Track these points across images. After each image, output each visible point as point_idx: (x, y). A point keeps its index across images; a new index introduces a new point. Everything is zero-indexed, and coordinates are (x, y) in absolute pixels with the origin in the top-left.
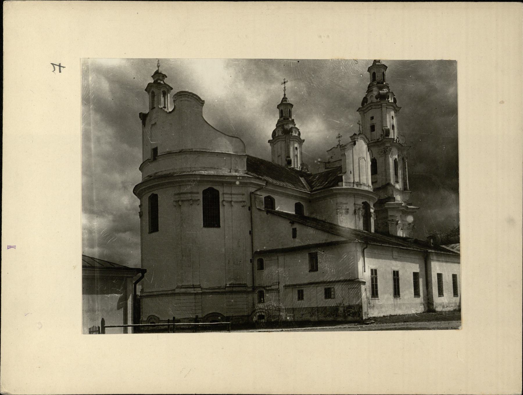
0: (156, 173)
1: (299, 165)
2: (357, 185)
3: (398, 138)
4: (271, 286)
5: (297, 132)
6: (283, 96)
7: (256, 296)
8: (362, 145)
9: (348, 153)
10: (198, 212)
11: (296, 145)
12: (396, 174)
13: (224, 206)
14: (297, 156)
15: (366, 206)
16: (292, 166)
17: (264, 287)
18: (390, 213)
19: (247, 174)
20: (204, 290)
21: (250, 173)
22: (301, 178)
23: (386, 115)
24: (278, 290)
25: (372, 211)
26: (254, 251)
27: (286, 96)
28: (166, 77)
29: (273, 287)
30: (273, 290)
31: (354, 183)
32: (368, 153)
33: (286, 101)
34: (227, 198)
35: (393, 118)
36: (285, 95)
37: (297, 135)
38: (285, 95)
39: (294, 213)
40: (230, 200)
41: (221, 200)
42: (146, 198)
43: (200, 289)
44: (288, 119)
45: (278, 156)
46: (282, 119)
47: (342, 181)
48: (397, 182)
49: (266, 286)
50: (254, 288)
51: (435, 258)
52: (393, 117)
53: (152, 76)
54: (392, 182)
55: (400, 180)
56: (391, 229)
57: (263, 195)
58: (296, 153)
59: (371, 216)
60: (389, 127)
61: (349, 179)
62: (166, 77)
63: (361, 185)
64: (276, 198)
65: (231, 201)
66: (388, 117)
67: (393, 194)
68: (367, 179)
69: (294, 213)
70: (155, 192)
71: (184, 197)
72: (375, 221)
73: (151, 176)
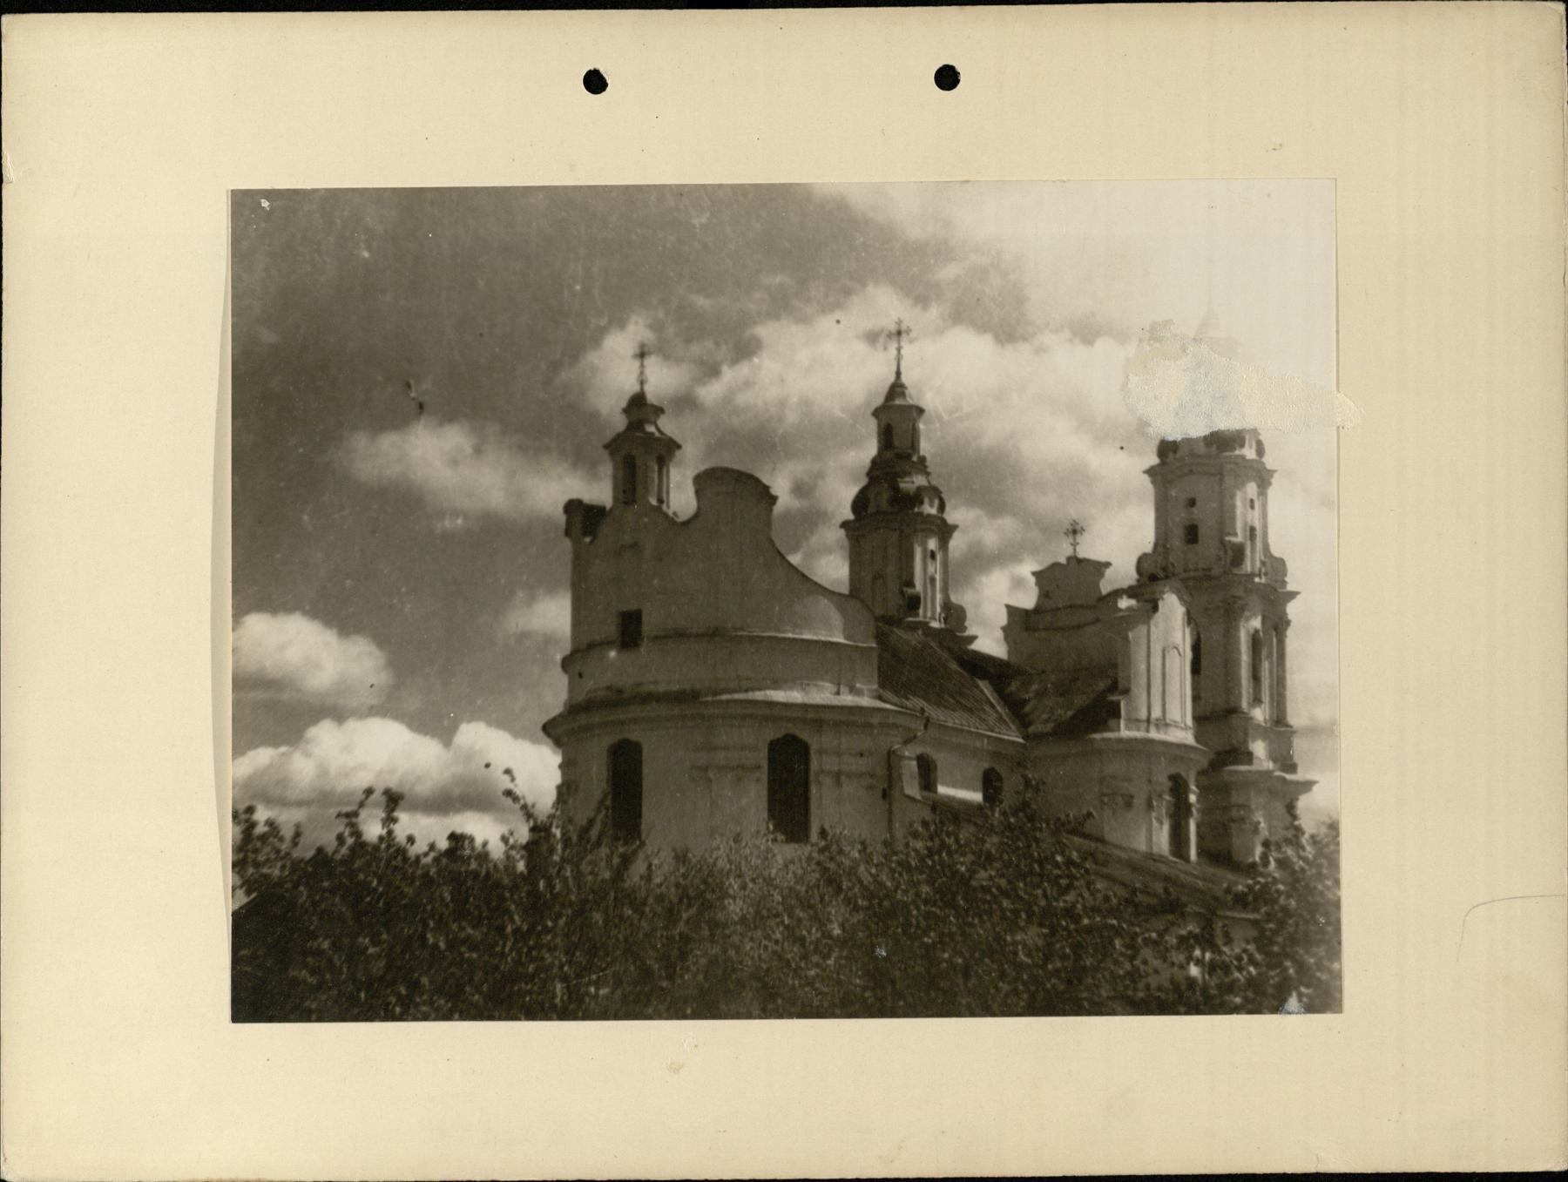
0: (639, 685)
1: (938, 609)
2: (1157, 726)
3: (1263, 563)
5: (937, 502)
6: (892, 379)
8: (1172, 607)
9: (1136, 634)
10: (752, 800)
11: (932, 544)
12: (1256, 677)
13: (820, 784)
14: (933, 580)
15: (1178, 787)
16: (920, 619)
18: (1236, 798)
19: (880, 698)
21: (888, 695)
23: (1233, 497)
25: (1193, 798)
27: (905, 379)
31: (1148, 721)
32: (1188, 631)
33: (903, 395)
34: (830, 763)
35: (1252, 507)
36: (898, 373)
37: (933, 511)
38: (898, 373)
39: (976, 797)
42: (597, 751)
44: (909, 457)
45: (875, 578)
46: (889, 455)
47: (1117, 715)
48: (1257, 700)
51: (1178, 584)
52: (1252, 501)
54: (1244, 705)
55: (1266, 697)
56: (1237, 842)
57: (910, 752)
58: (931, 569)
59: (1188, 813)
60: (1239, 539)
61: (1137, 710)
63: (1167, 725)
64: (941, 758)
66: (1239, 503)
67: (1245, 742)
68: (1183, 716)
69: (976, 797)
70: (634, 735)
71: (720, 757)
72: (1198, 826)
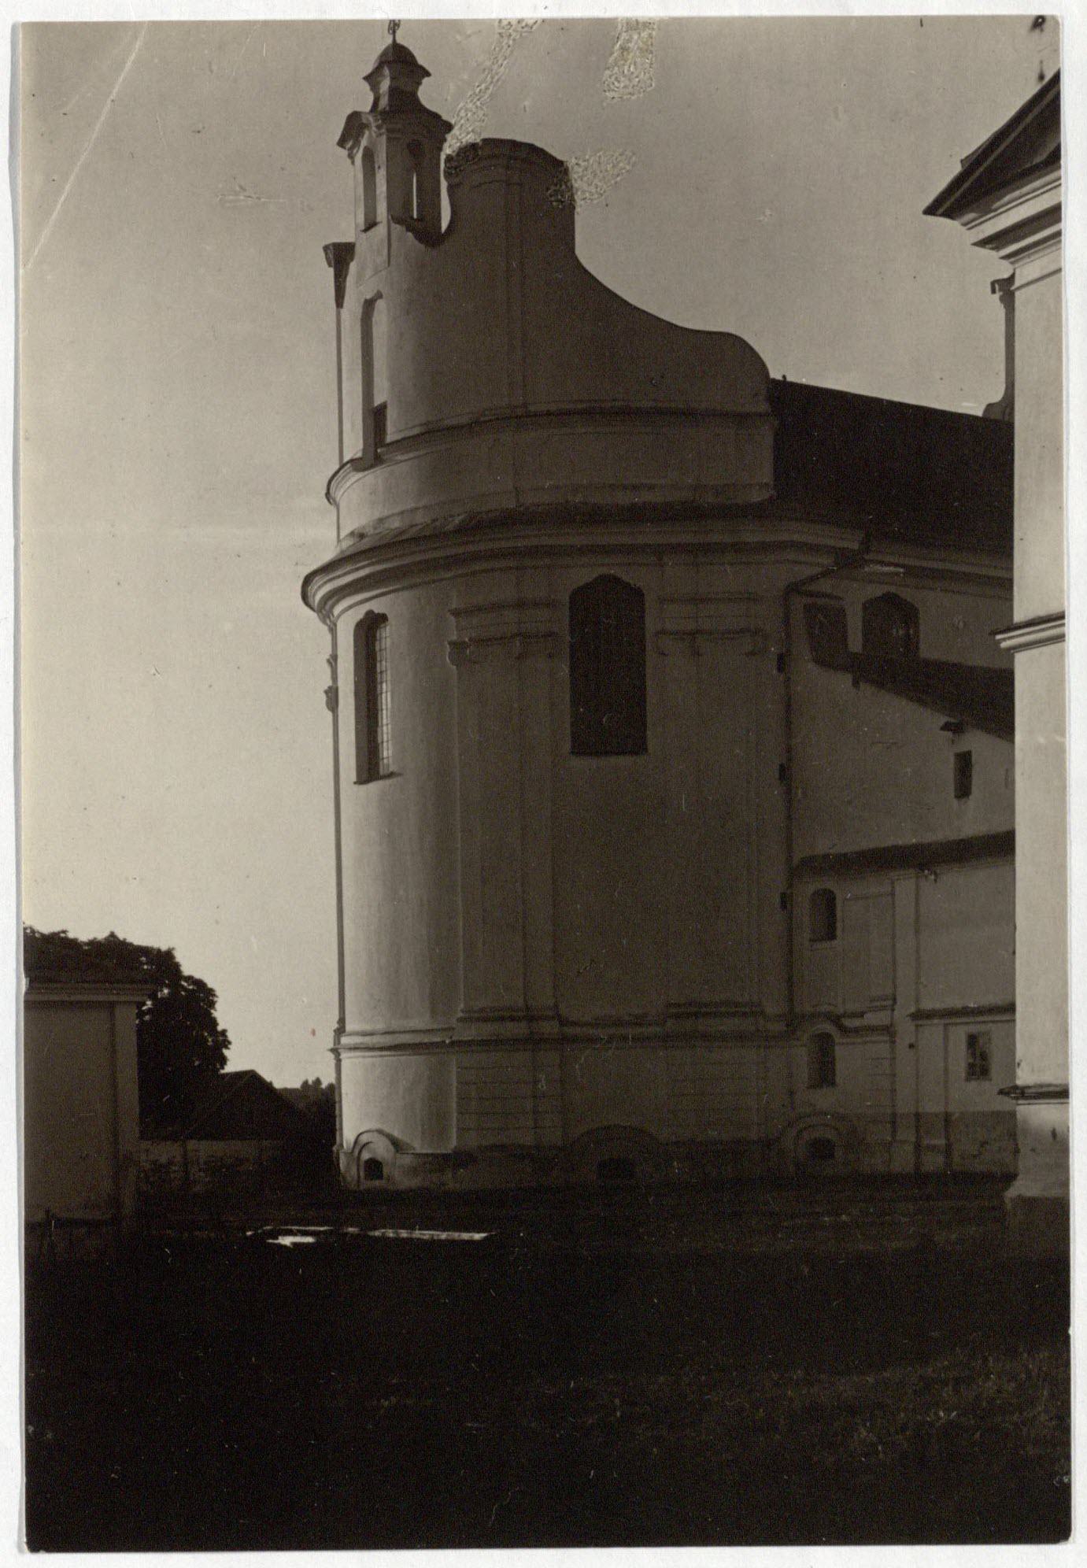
4: (862, 1015)
7: (801, 1055)
17: (836, 1020)
20: (569, 1031)
22: (483, 1235)
24: (889, 1030)
26: (796, 861)
28: (428, 74)
29: (871, 1019)
30: (872, 1029)
40: (691, 626)
41: (651, 625)
43: (556, 1023)
49: (844, 1015)
50: (793, 1021)
53: (367, 78)
62: (428, 74)
65: (693, 634)
70: (830, 885)
73: (362, 536)
